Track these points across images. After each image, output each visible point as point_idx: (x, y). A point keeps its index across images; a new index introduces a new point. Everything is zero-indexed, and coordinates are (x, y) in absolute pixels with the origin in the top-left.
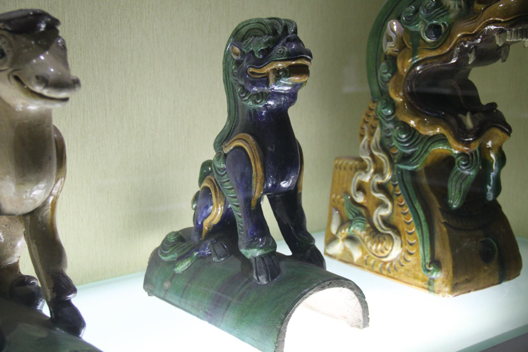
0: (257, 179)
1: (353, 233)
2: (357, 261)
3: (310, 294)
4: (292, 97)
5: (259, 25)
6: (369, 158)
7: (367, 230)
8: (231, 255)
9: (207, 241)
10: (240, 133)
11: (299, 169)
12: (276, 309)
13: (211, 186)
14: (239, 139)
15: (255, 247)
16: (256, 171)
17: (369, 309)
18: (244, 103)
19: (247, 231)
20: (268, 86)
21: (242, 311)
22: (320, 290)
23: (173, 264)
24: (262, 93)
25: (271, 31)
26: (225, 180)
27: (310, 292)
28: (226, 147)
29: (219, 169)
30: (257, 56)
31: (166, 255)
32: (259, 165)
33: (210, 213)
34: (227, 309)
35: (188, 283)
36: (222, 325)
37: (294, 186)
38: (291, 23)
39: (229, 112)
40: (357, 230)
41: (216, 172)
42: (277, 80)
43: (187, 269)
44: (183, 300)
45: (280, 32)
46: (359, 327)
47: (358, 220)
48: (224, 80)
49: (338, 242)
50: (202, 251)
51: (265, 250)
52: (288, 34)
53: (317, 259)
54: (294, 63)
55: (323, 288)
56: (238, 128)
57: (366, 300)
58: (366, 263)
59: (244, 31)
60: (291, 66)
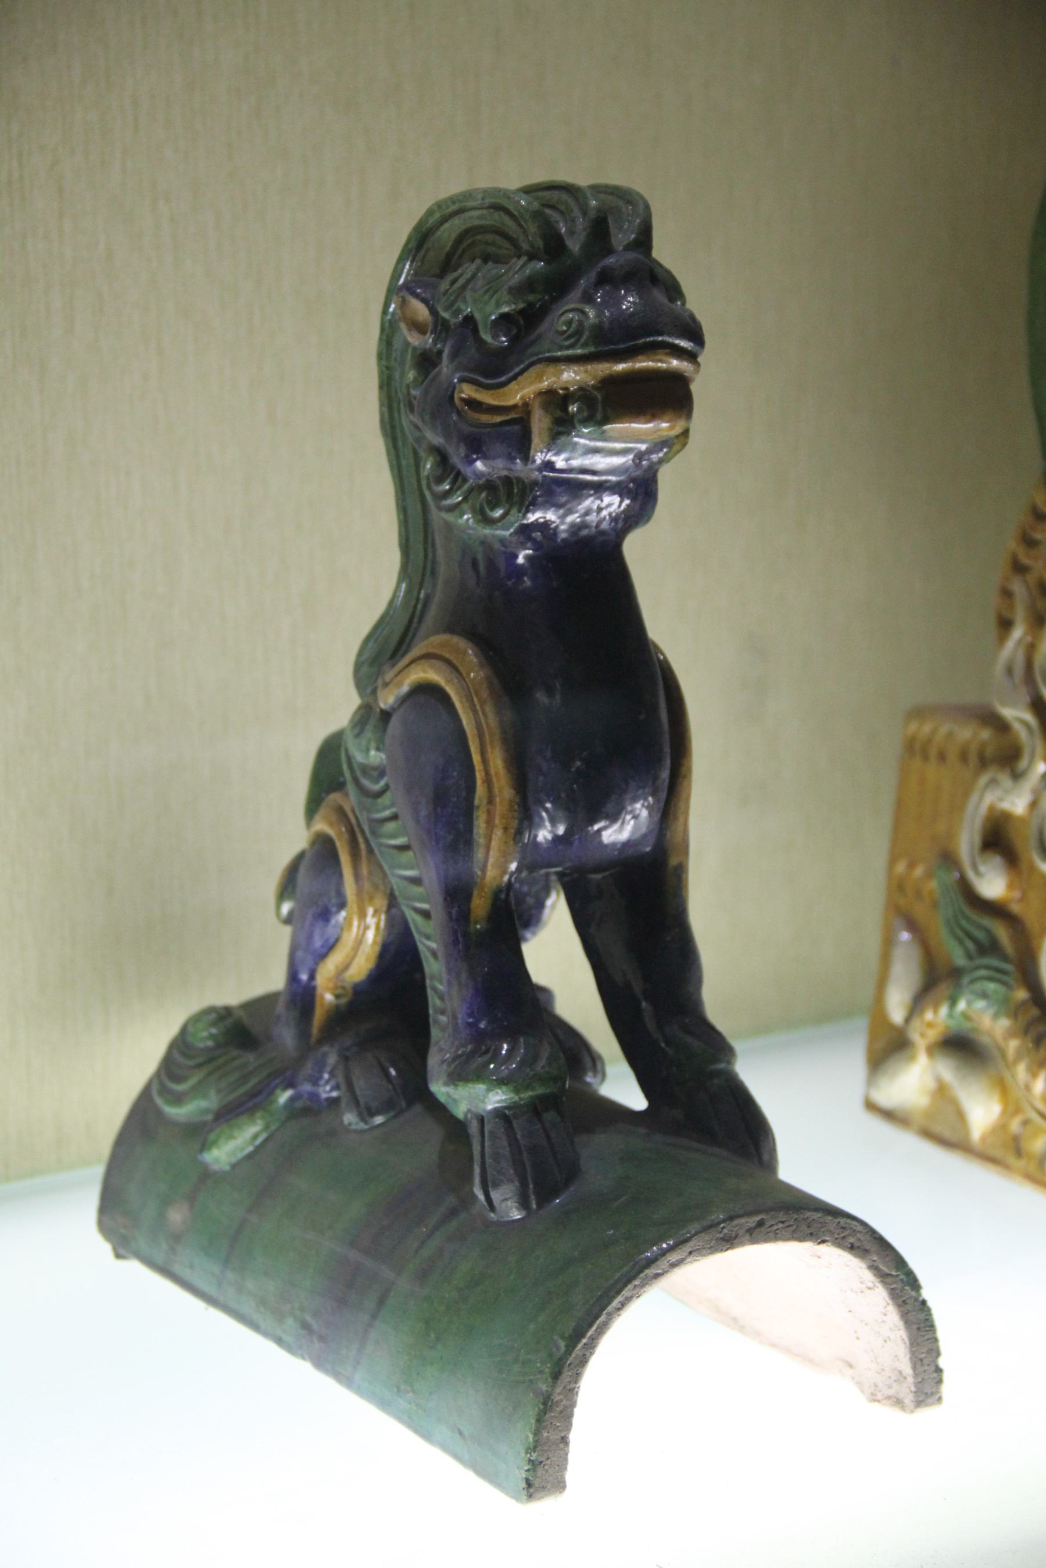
0: (490, 814)
1: (967, 1025)
2: (983, 1139)
3: (674, 1265)
4: (641, 490)
5: (496, 219)
6: (1029, 717)
7: (1016, 1012)
8: (410, 1104)
9: (325, 1049)
10: (437, 632)
11: (665, 775)
12: (542, 1318)
13: (340, 834)
14: (427, 656)
15: (479, 1075)
16: (488, 781)
17: (941, 1333)
18: (449, 517)
19: (455, 1017)
20: (527, 458)
21: (427, 1323)
22: (714, 1250)
23: (199, 1133)
24: (508, 481)
25: (540, 243)
26: (387, 813)
27: (674, 1257)
28: (386, 685)
29: (366, 770)
30: (487, 337)
31: (178, 1099)
32: (497, 761)
33: (337, 940)
34: (374, 1316)
35: (250, 1210)
36: (357, 1377)
37: (652, 840)
38: (629, 202)
39: (405, 547)
40: (982, 1012)
41: (356, 781)
42: (559, 434)
43: (250, 1156)
44: (230, 1275)
45: (574, 245)
46: (898, 1403)
47: (983, 972)
48: (382, 421)
49: (912, 1058)
50: (307, 1087)
51: (517, 1091)
52: (610, 251)
53: (744, 1130)
54: (621, 367)
55: (729, 1242)
56: (433, 611)
57: (926, 1294)
58: (1017, 1146)
59: (448, 233)
60: (610, 382)
